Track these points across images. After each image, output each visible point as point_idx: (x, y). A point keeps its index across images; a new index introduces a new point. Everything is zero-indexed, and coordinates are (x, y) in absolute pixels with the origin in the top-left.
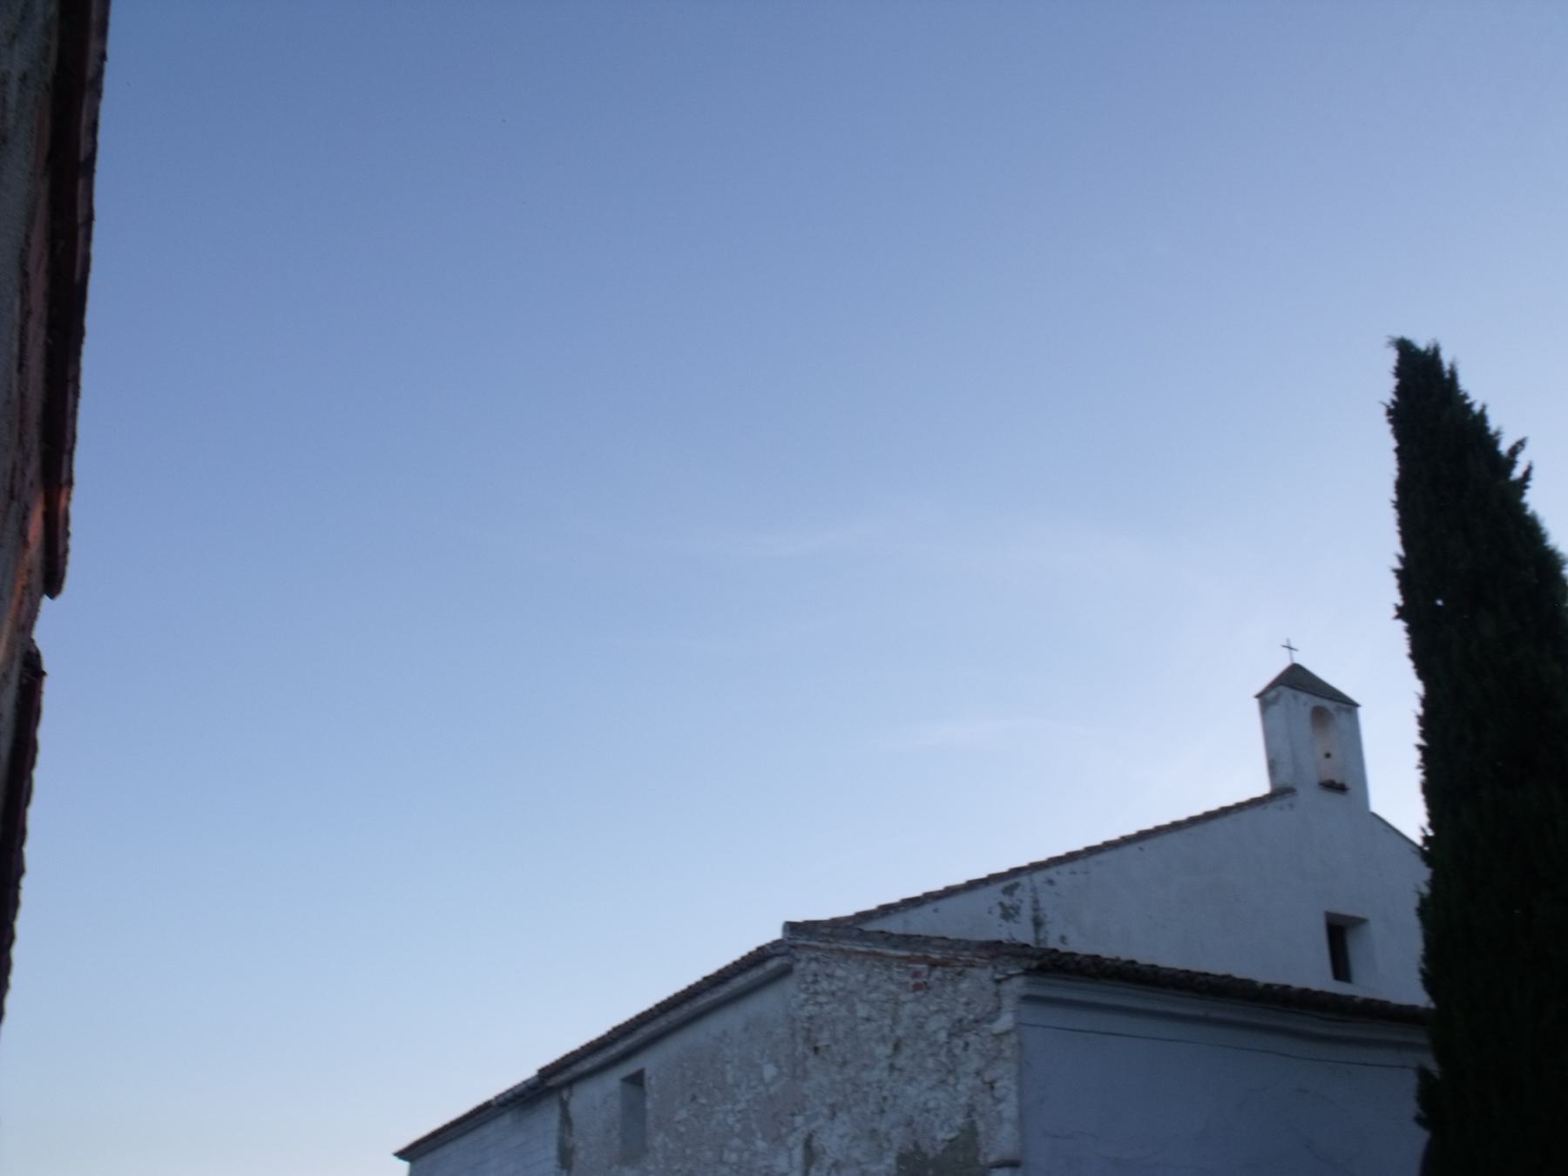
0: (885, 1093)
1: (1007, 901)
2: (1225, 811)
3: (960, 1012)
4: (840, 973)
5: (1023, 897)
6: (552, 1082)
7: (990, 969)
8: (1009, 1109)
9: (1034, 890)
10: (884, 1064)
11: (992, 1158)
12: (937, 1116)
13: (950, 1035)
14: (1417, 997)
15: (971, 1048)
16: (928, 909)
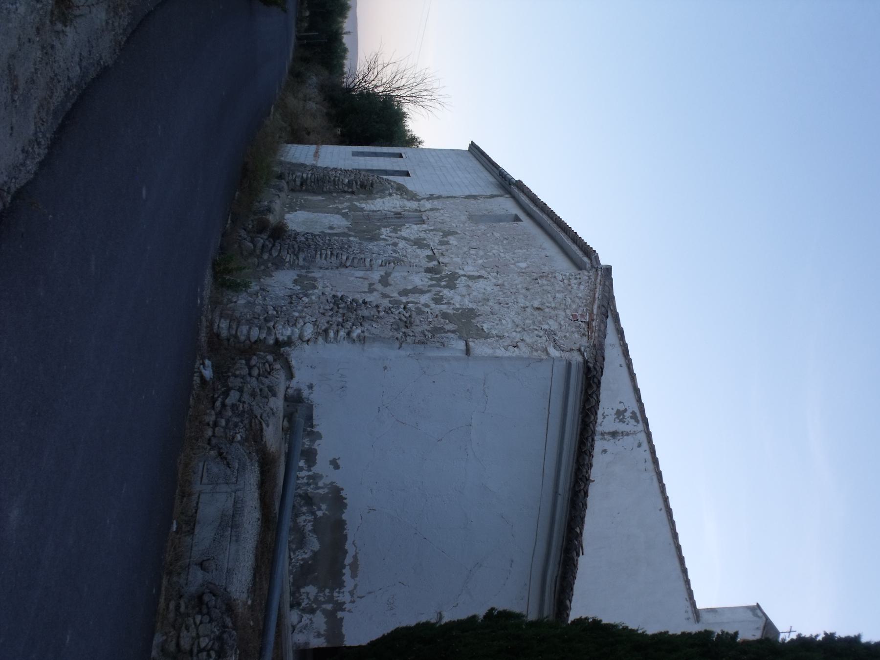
0: (510, 304)
1: (628, 414)
2: (685, 571)
3: (559, 334)
4: (582, 287)
5: (630, 426)
6: (515, 189)
7: (587, 344)
8: (501, 352)
9: (635, 433)
10: (528, 304)
11: (471, 344)
12: (497, 324)
13: (546, 330)
14: (573, 616)
15: (538, 338)
16: (622, 360)
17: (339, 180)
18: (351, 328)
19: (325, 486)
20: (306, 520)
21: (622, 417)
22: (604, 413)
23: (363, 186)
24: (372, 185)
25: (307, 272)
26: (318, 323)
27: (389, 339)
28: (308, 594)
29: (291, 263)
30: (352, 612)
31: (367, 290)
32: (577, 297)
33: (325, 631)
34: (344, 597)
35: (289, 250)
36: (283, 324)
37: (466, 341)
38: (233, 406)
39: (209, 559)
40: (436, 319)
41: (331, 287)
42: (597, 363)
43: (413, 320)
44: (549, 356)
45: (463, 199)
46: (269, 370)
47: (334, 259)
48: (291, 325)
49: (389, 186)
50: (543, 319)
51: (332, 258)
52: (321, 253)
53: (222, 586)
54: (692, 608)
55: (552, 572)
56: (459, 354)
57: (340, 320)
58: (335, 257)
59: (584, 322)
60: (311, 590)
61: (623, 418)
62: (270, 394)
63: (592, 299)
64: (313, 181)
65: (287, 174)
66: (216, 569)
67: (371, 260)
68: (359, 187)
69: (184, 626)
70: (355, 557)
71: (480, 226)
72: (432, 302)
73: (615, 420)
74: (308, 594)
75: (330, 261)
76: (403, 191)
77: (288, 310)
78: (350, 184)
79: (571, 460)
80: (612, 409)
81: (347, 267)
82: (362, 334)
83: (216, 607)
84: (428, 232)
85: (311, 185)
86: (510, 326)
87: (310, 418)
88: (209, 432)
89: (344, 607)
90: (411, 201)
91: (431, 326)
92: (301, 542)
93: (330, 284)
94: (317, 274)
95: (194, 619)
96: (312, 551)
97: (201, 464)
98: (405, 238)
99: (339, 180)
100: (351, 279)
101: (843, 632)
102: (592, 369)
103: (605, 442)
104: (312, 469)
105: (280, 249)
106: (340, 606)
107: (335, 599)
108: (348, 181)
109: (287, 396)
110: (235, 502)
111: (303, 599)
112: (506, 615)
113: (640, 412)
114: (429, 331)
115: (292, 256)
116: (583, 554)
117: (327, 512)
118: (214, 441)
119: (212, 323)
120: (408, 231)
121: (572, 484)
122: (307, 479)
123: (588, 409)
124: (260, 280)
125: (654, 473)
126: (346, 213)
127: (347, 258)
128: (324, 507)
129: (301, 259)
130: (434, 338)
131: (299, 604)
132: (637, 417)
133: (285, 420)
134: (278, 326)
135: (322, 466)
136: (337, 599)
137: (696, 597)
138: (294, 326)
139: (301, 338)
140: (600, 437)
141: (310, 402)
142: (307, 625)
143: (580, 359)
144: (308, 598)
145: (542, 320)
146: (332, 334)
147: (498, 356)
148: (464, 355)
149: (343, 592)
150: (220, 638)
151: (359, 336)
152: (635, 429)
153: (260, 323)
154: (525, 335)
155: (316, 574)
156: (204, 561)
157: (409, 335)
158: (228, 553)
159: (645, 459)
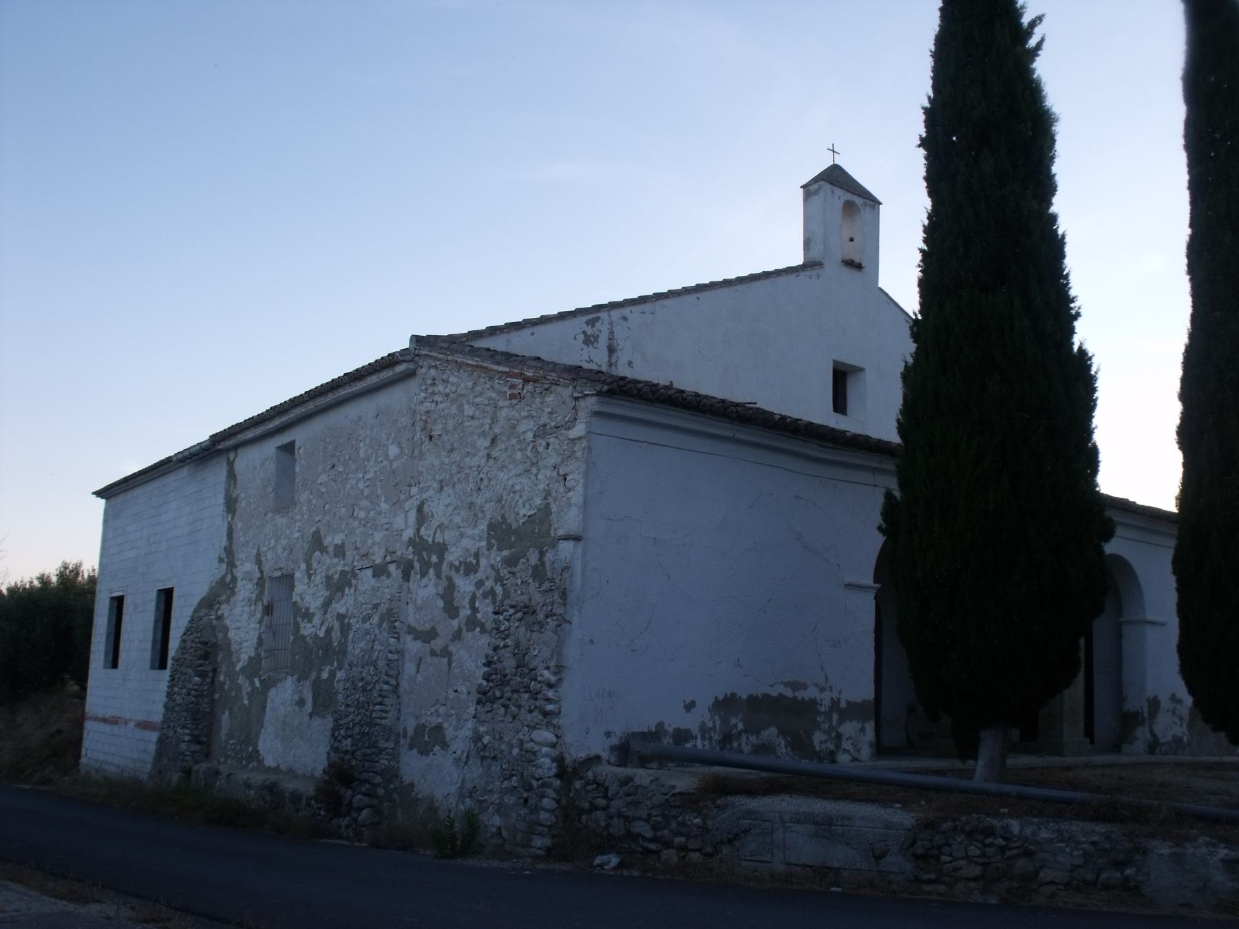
1: (589, 331)
5: (602, 328)
8: (577, 497)
9: (611, 323)
11: (561, 532)
14: (894, 437)
16: (527, 332)
17: (196, 690)
18: (540, 682)
19: (712, 718)
20: (746, 743)
21: (592, 339)
22: (586, 360)
23: (206, 656)
24: (205, 644)
25: (405, 735)
26: (532, 724)
27: (559, 636)
28: (821, 742)
29: (391, 757)
30: (841, 690)
31: (445, 660)
32: (472, 388)
33: (858, 723)
34: (826, 699)
35: (375, 760)
36: (534, 768)
37: (559, 540)
38: (655, 828)
39: (872, 850)
40: (517, 574)
41: (439, 706)
42: (602, 379)
43: (521, 604)
44: (584, 437)
45: (236, 518)
46: (595, 786)
47: (387, 701)
48: (534, 758)
49: (205, 620)
50: (515, 438)
51: (387, 703)
52: (379, 718)
53: (905, 834)
54: (807, 270)
55: (812, 450)
56: (579, 550)
57: (526, 696)
58: (386, 699)
59: (523, 385)
60: (818, 737)
61: (593, 336)
62: (631, 784)
63: (478, 370)
64: (195, 727)
65: (184, 763)
66: (885, 841)
67: (390, 652)
68: (207, 662)
69: (953, 874)
70: (787, 684)
71: (302, 500)
72: (472, 577)
73: (595, 348)
74: (821, 742)
75: (389, 706)
76: (215, 600)
77: (508, 762)
78: (202, 675)
79: (650, 408)
80: (582, 349)
81: (398, 684)
82: (552, 669)
83: (931, 841)
84: (311, 572)
85: (201, 730)
86: (525, 481)
87: (645, 736)
88: (695, 856)
89: (836, 700)
90: (236, 590)
91: (531, 580)
92: (766, 748)
93: (433, 706)
94: (411, 725)
95: (945, 863)
96: (778, 736)
97: (744, 863)
98: (325, 602)
99: (196, 690)
100: (419, 678)
101: (918, 127)
102: (610, 387)
103: (619, 364)
104: (694, 734)
105: (373, 772)
106: (835, 703)
107: (827, 709)
108: (198, 676)
109: (617, 763)
110: (798, 822)
111: (827, 748)
112: (1175, 562)
113: (587, 314)
114: (540, 585)
115: (381, 756)
116: (756, 403)
117: (739, 718)
118: (709, 849)
119: (536, 858)
120: (308, 598)
121: (722, 420)
122: (705, 741)
123: (653, 395)
124: (420, 800)
125: (657, 303)
126: (262, 682)
127: (387, 683)
128: (733, 721)
129: (386, 745)
130: (553, 579)
131: (832, 753)
132: (593, 318)
133: (648, 766)
134: (539, 775)
135: (691, 723)
136: (827, 707)
137: (794, 265)
138: (536, 754)
139: (553, 746)
140: (613, 368)
141: (624, 736)
142: (852, 744)
143: (593, 400)
144: (826, 741)
145: (517, 439)
146: (550, 707)
147: (582, 501)
148: (581, 544)
149: (821, 700)
150: (970, 835)
151: (555, 673)
152: (606, 322)
153: (534, 796)
154: (547, 464)
155: (801, 732)
156: (874, 856)
157: (551, 611)
158: (865, 829)
159: (641, 313)
